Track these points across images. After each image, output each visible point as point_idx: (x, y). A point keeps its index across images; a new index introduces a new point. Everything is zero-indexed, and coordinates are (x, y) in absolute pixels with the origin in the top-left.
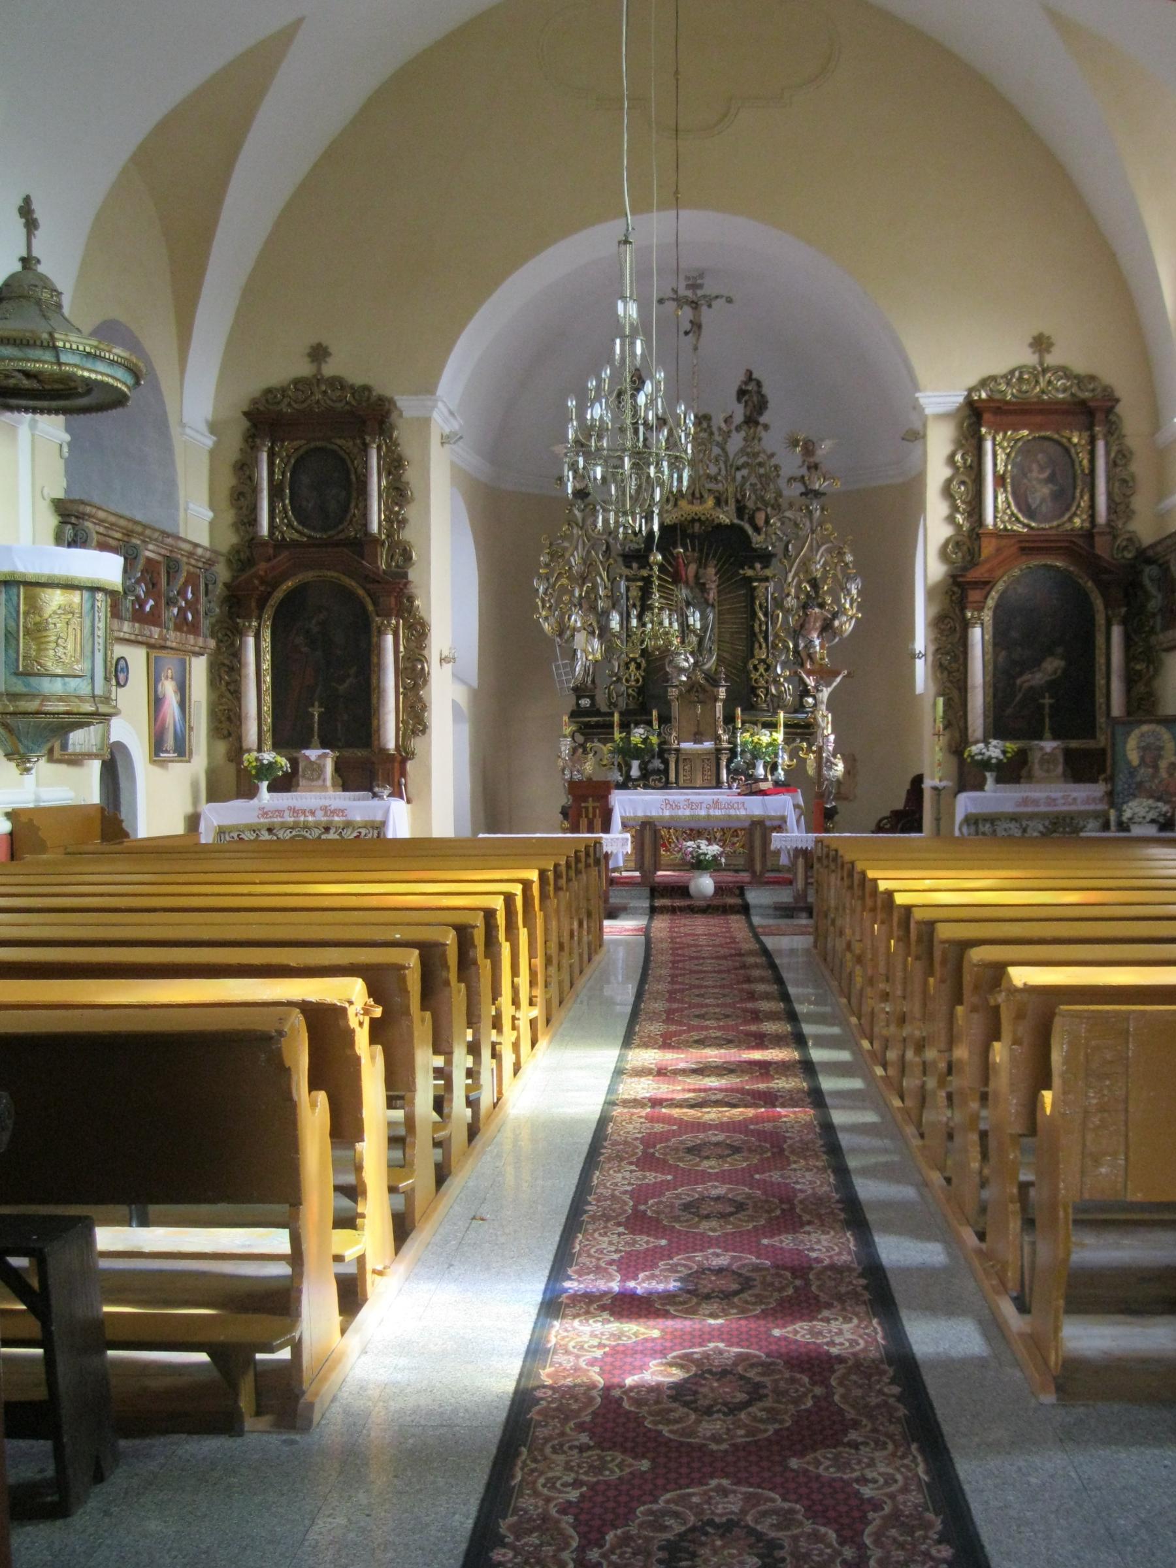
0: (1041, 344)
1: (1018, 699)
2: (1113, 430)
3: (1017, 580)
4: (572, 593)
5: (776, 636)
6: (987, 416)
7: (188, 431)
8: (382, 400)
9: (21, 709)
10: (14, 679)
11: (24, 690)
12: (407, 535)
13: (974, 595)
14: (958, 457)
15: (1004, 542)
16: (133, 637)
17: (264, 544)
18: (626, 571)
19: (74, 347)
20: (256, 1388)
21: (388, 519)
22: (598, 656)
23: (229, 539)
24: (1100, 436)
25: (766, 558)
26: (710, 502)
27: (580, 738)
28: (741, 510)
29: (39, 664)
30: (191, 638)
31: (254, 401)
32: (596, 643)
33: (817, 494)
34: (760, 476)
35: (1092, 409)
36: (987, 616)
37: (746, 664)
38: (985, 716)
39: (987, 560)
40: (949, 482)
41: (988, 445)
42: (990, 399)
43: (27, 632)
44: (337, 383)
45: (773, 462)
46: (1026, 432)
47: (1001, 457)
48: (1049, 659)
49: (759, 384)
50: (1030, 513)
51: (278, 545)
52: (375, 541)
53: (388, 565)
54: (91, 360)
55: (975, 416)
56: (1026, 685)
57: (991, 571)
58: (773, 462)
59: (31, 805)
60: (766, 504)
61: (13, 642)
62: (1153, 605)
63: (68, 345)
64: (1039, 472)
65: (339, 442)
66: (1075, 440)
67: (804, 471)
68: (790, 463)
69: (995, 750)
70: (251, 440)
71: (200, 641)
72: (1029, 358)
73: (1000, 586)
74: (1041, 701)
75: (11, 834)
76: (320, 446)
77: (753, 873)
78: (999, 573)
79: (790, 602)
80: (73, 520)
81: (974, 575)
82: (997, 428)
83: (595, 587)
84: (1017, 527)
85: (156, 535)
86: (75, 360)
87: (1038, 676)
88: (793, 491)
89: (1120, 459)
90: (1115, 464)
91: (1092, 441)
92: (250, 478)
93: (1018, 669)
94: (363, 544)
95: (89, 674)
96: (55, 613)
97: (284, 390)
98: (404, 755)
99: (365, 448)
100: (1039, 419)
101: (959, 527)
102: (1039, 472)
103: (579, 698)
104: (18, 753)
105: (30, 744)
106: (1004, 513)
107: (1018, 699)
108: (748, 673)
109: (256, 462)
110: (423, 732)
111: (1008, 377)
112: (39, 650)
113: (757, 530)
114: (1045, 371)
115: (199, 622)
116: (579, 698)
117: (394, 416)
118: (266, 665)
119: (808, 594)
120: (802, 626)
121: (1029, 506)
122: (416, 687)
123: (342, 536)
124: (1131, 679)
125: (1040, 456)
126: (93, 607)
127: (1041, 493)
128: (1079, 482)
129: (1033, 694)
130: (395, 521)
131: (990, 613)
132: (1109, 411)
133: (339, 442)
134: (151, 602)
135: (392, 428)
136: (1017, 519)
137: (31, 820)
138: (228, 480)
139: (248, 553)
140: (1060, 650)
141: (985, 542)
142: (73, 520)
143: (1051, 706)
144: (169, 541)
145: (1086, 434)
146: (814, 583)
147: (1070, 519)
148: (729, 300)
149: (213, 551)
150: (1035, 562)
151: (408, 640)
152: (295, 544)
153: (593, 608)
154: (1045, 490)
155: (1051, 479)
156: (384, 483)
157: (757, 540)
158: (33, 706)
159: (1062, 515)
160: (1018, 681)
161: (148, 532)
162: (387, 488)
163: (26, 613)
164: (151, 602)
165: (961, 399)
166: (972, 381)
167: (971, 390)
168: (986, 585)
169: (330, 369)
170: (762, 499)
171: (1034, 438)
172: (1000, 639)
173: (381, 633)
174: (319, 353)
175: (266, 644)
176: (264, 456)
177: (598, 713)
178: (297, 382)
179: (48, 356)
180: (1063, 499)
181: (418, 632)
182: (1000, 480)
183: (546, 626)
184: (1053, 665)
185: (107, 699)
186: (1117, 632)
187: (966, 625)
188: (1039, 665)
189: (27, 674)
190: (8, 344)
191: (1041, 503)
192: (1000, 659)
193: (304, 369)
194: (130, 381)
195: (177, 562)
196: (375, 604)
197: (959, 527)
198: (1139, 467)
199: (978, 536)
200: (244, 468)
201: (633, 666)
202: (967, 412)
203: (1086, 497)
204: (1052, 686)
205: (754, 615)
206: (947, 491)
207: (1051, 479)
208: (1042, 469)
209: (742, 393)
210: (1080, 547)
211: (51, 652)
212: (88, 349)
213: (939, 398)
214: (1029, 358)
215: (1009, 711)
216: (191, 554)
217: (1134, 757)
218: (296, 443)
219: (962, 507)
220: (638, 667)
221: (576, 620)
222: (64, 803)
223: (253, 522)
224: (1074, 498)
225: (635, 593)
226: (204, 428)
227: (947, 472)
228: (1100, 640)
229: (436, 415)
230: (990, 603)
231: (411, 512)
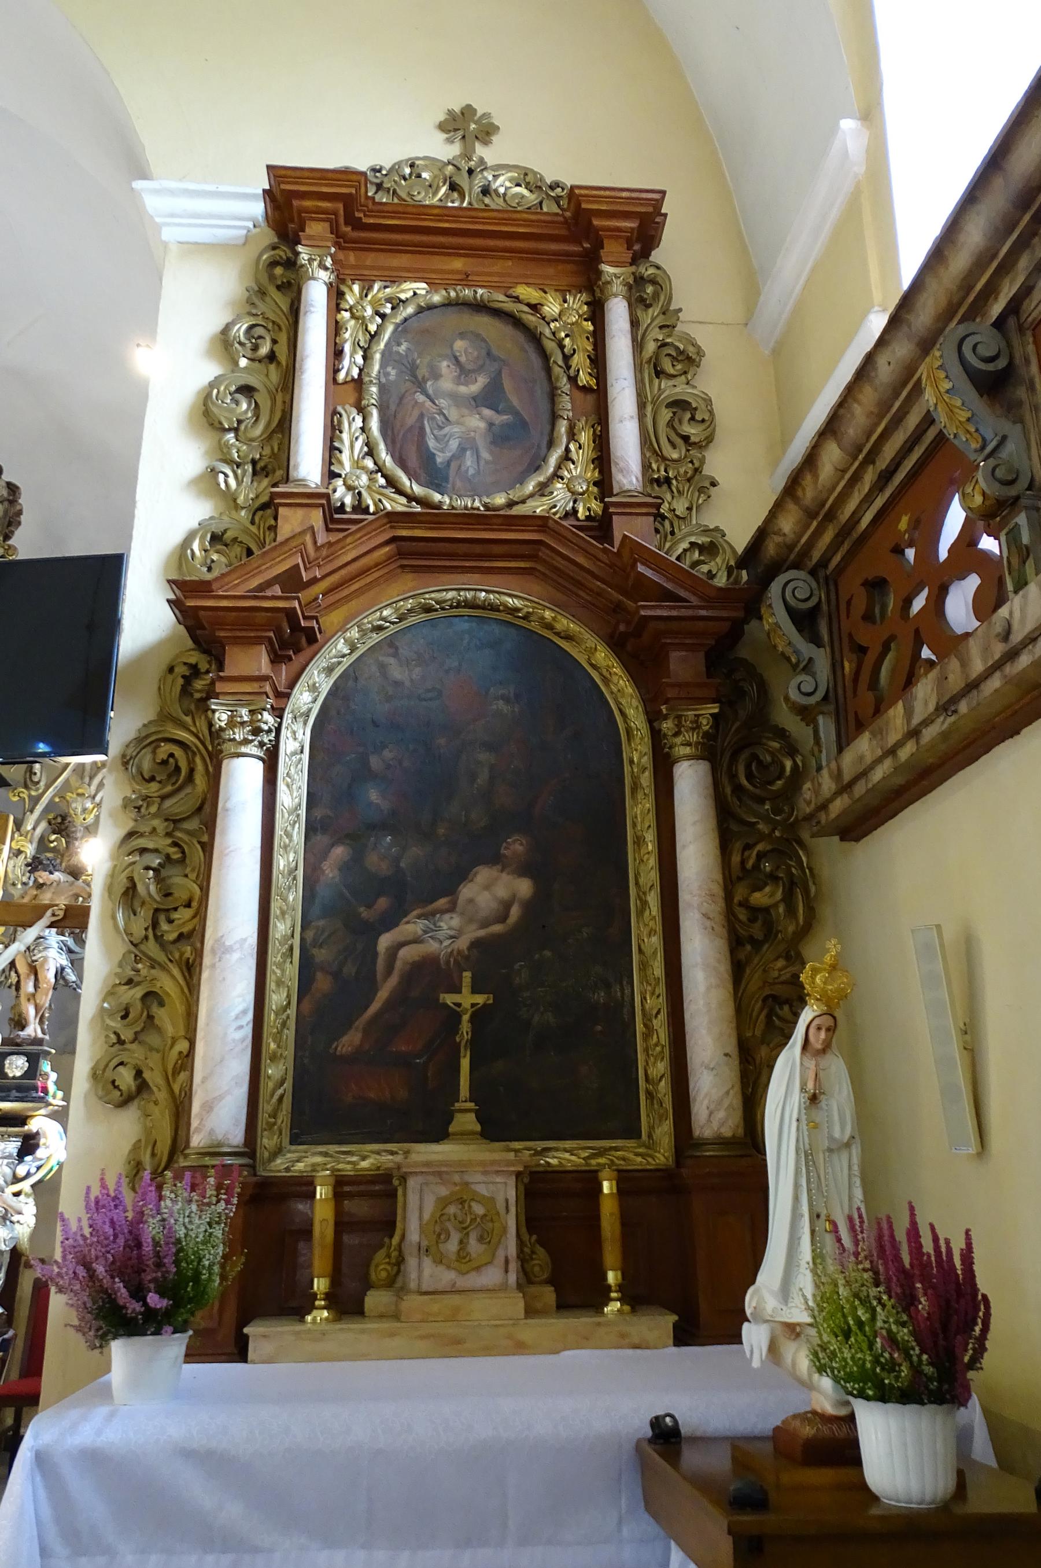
0: (466, 126)
1: (383, 994)
2: (647, 292)
20: (615, 1348)
24: (617, 287)
35: (596, 238)
41: (316, 293)
46: (421, 287)
48: (483, 874)
56: (406, 954)
62: (793, 689)
64: (458, 382)
66: (552, 307)
70: (277, 282)
72: (443, 149)
74: (449, 999)
87: (449, 923)
89: (668, 359)
91: (597, 313)
93: (383, 903)
101: (230, 499)
102: (458, 382)
106: (357, 465)
107: (383, 994)
121: (428, 458)
125: (459, 345)
127: (459, 428)
128: (565, 404)
129: (431, 975)
131: (305, 735)
136: (391, 482)
140: (516, 846)
143: (479, 1015)
147: (543, 490)
150: (446, 591)
154: (476, 423)
155: (490, 398)
159: (522, 480)
160: (385, 941)
171: (448, 304)
180: (523, 442)
184: (493, 891)
186: (690, 781)
188: (451, 891)
191: (462, 450)
192: (330, 871)
197: (230, 499)
203: (584, 437)
204: (488, 958)
207: (490, 398)
208: (464, 373)
214: (443, 149)
215: (349, 1042)
228: (640, 810)
230: (302, 698)
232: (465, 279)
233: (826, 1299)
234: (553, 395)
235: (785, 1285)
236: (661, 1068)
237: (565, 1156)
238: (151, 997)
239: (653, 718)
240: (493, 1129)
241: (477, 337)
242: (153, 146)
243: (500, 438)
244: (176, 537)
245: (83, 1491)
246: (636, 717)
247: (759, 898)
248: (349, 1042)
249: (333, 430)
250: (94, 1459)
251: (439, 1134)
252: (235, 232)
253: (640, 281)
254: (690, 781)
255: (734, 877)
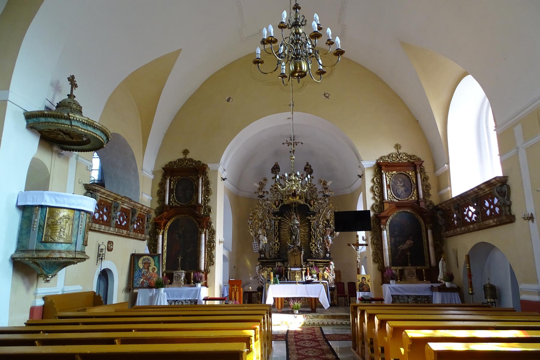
0: (397, 147)
2: (422, 171)
3: (396, 216)
4: (259, 224)
5: (317, 236)
6: (383, 167)
7: (144, 172)
8: (203, 165)
9: (40, 256)
10: (40, 244)
11: (43, 248)
12: (210, 204)
13: (383, 221)
14: (375, 180)
15: (391, 205)
16: (115, 233)
17: (166, 207)
18: (274, 218)
19: (78, 119)
21: (204, 200)
22: (266, 242)
23: (156, 205)
25: (314, 214)
26: (298, 198)
27: (261, 266)
28: (306, 200)
29: (51, 238)
30: (140, 235)
31: (166, 165)
32: (266, 238)
33: (327, 196)
34: (311, 191)
35: (415, 164)
36: (387, 228)
37: (309, 244)
38: (389, 259)
39: (387, 210)
40: (372, 187)
41: (384, 176)
42: (383, 162)
43: (48, 225)
44: (191, 160)
45: (315, 187)
47: (388, 179)
49: (310, 166)
50: (398, 196)
51: (171, 207)
52: (200, 206)
53: (204, 213)
54: (85, 126)
55: (380, 167)
57: (388, 213)
58: (315, 187)
59: (60, 293)
60: (313, 198)
61: (41, 229)
63: (75, 119)
65: (191, 177)
66: (411, 174)
67: (323, 190)
68: (319, 188)
69: (395, 270)
71: (143, 236)
72: (394, 151)
73: (391, 218)
75: (43, 306)
76: (185, 179)
77: (312, 308)
78: (390, 214)
79: (321, 226)
80: (91, 191)
81: (383, 214)
82: (386, 171)
83: (265, 222)
84: (395, 200)
85: (127, 200)
86: (79, 124)
87: (405, 246)
88: (320, 196)
89: (425, 179)
90: (424, 181)
91: (416, 174)
92: (164, 188)
94: (197, 206)
95: (74, 243)
96: (61, 218)
97: (175, 162)
98: (207, 272)
99: (198, 178)
100: (399, 168)
103: (261, 254)
104: (43, 274)
105: (48, 271)
108: (310, 247)
109: (165, 183)
110: (213, 265)
111: (388, 156)
112: (52, 233)
113: (311, 206)
114: (399, 155)
115: (144, 230)
116: (261, 254)
117: (207, 170)
118: (165, 244)
119: (326, 224)
120: (325, 233)
121: (398, 194)
122: (211, 250)
123: (190, 204)
124: (436, 247)
126: (79, 217)
127: (401, 190)
129: (404, 251)
130: (206, 200)
132: (421, 165)
133: (191, 177)
134: (125, 222)
135: (206, 173)
137: (52, 300)
138: (157, 188)
139: (162, 209)
141: (385, 204)
142: (91, 191)
144: (132, 203)
145: (413, 172)
146: (328, 221)
147: (411, 198)
148: (302, 143)
149: (151, 208)
150: (400, 211)
151: (209, 236)
152: (176, 207)
153: (265, 228)
156: (203, 189)
157: (312, 209)
158: (45, 255)
161: (123, 199)
162: (204, 190)
163: (48, 218)
164: (125, 222)
165: (375, 163)
166: (378, 158)
167: (377, 160)
168: (386, 217)
169: (188, 157)
170: (312, 197)
172: (392, 235)
173: (201, 234)
174: (186, 152)
175: (166, 237)
176: (168, 181)
177: (266, 259)
178: (179, 160)
179: (68, 122)
180: (409, 191)
181: (213, 233)
182: (388, 186)
183: (251, 234)
184: (409, 242)
185: (83, 252)
186: (429, 231)
187: (381, 230)
189: (46, 242)
190: (51, 117)
192: (392, 241)
193: (182, 156)
194: (105, 138)
195: (135, 210)
196: (199, 225)
198: (431, 181)
199: (383, 203)
200: (162, 185)
201: (276, 245)
202: (376, 167)
205: (310, 230)
206: (372, 190)
207: (404, 186)
208: (401, 183)
209: (305, 169)
210: (415, 206)
211: (58, 234)
212: (83, 121)
213: (368, 163)
214: (394, 151)
215: (396, 257)
216: (141, 209)
217: (141, 266)
218: (178, 177)
219: (377, 194)
220: (278, 245)
221: (260, 232)
222: (80, 291)
223: (164, 200)
224: (412, 191)
225: (277, 224)
226: (151, 172)
227: (372, 184)
228: (424, 234)
229: (220, 170)
230: (388, 223)
231: (211, 197)
232: (400, 170)
233: (444, 277)
234: (411, 185)
235: (440, 277)
236: (427, 260)
237: (419, 268)
238: (378, 253)
239: (425, 224)
240: (412, 266)
241: (400, 177)
242: (363, 158)
243: (406, 191)
244: (371, 205)
245: (392, 289)
246: (423, 224)
247: (437, 243)
248: (396, 257)
249: (387, 191)
250: (392, 287)
251: (407, 266)
252: (372, 165)
253: (421, 169)
254: (429, 231)
255: (434, 240)
